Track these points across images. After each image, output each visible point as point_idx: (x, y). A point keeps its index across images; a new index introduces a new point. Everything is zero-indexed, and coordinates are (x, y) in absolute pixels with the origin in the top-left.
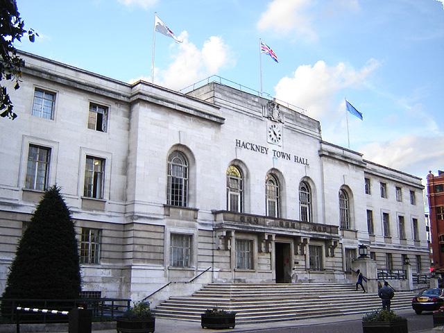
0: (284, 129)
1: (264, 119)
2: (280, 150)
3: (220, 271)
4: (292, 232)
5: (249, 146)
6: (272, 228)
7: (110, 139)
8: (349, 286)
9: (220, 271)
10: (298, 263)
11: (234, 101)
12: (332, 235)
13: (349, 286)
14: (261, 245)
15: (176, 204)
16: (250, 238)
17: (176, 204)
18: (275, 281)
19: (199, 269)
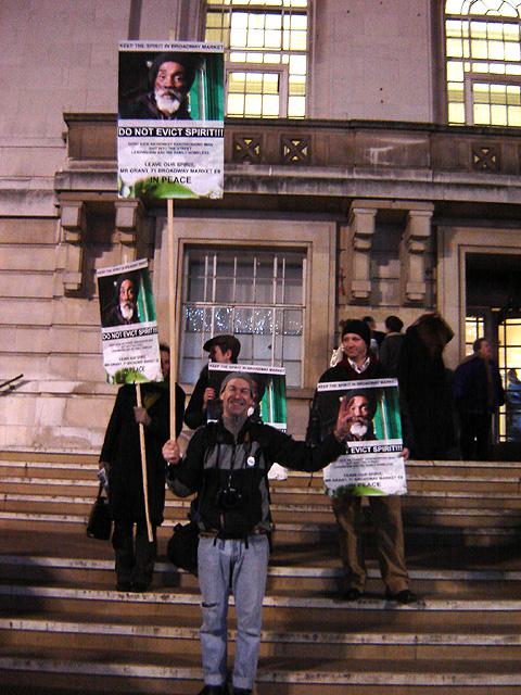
16: (286, 231)
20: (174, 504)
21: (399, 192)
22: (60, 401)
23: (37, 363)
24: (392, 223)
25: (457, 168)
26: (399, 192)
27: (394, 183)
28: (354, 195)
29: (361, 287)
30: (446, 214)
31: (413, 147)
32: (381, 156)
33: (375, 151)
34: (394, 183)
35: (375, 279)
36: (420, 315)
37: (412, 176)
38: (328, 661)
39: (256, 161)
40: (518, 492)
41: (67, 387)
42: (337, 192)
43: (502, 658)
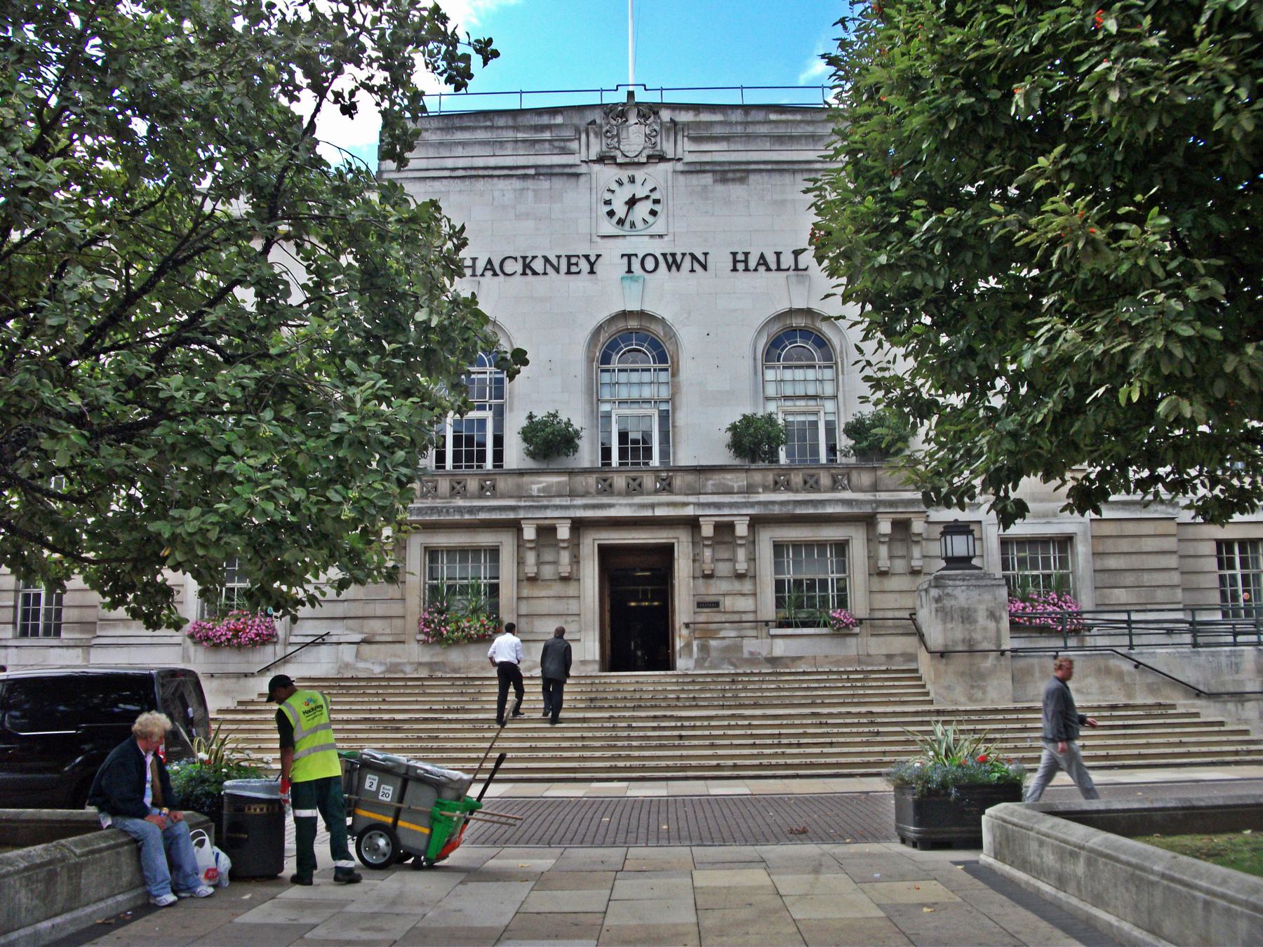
0: (681, 178)
1: (583, 169)
2: (658, 248)
3: (365, 641)
4: (653, 506)
5: (538, 265)
6: (557, 501)
7: (408, 268)
8: (105, 606)
9: (365, 641)
10: (716, 604)
11: (459, 151)
12: (883, 496)
13: (105, 606)
14: (877, 551)
15: (469, 457)
16: (485, 539)
17: (469, 457)
18: (597, 667)
19: (293, 639)
20: (268, 757)
21: (549, 514)
22: (355, 646)
23: (339, 623)
24: (545, 532)
25: (586, 494)
26: (549, 514)
27: (546, 507)
28: (521, 516)
29: (531, 569)
30: (579, 526)
31: (559, 483)
32: (539, 490)
33: (535, 487)
34: (546, 507)
35: (539, 563)
36: (269, 679)
37: (557, 501)
38: (663, 870)
39: (464, 497)
40: (1258, 633)
41: (357, 638)
42: (512, 516)
43: (673, 880)
